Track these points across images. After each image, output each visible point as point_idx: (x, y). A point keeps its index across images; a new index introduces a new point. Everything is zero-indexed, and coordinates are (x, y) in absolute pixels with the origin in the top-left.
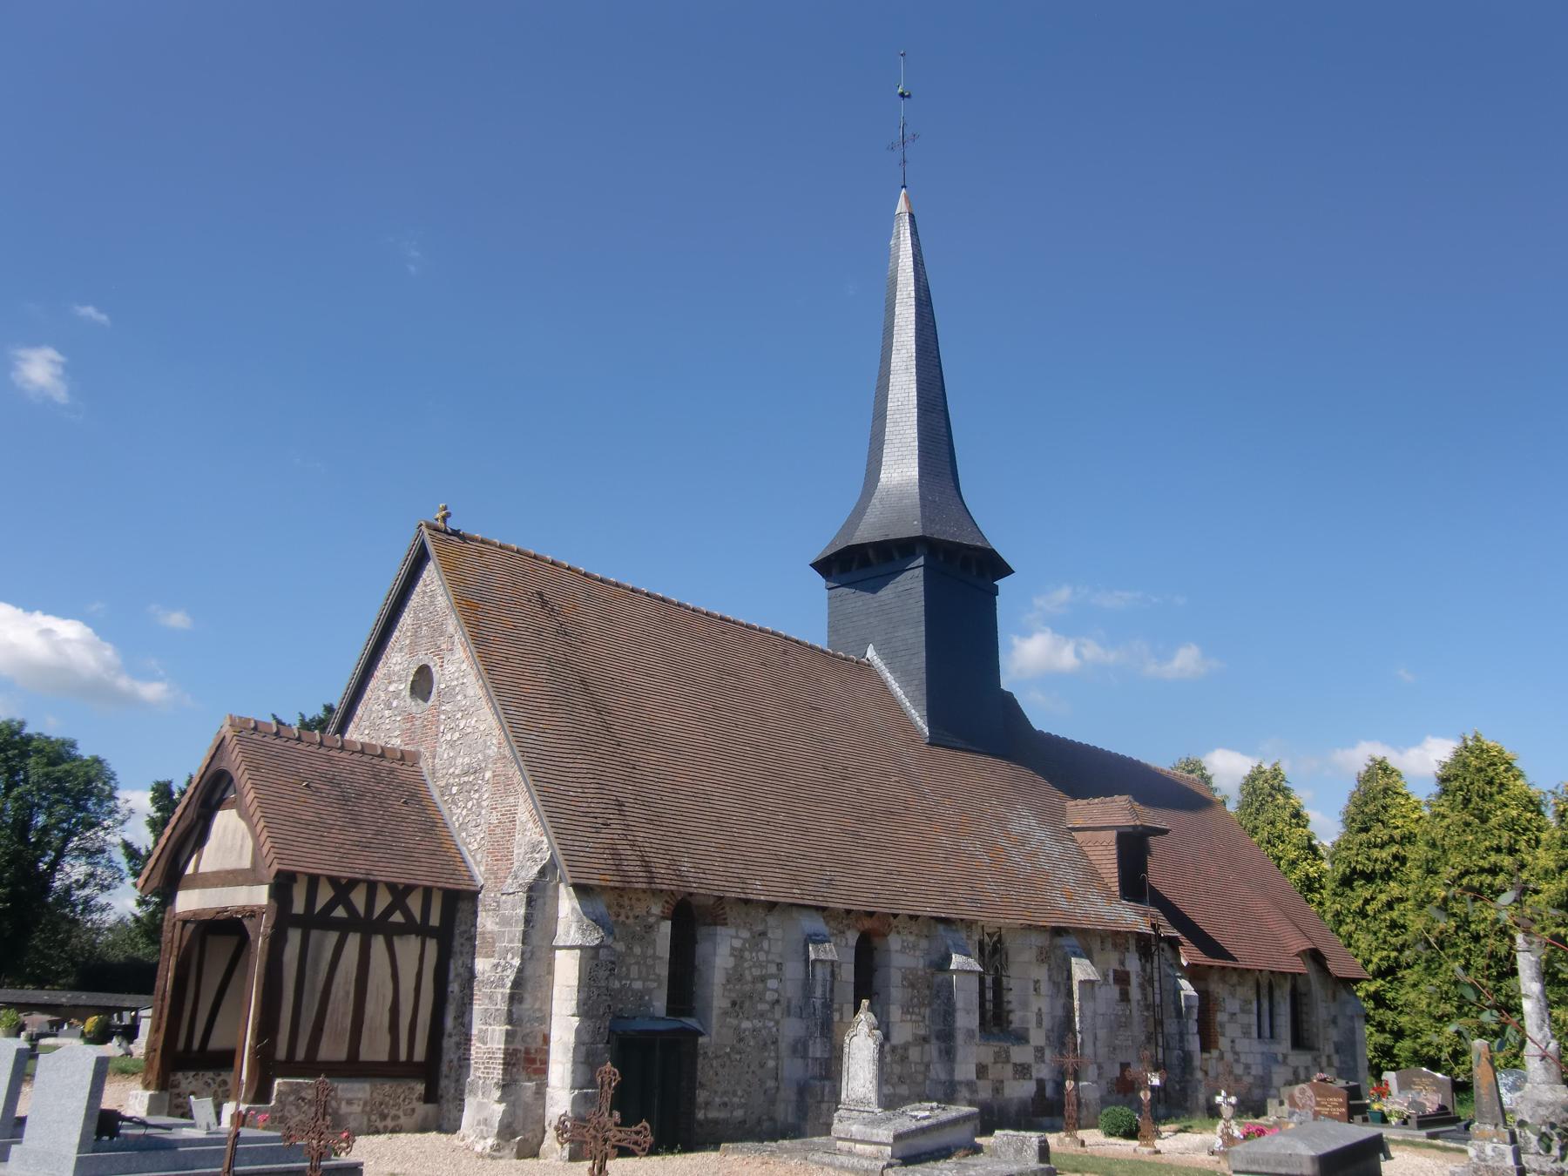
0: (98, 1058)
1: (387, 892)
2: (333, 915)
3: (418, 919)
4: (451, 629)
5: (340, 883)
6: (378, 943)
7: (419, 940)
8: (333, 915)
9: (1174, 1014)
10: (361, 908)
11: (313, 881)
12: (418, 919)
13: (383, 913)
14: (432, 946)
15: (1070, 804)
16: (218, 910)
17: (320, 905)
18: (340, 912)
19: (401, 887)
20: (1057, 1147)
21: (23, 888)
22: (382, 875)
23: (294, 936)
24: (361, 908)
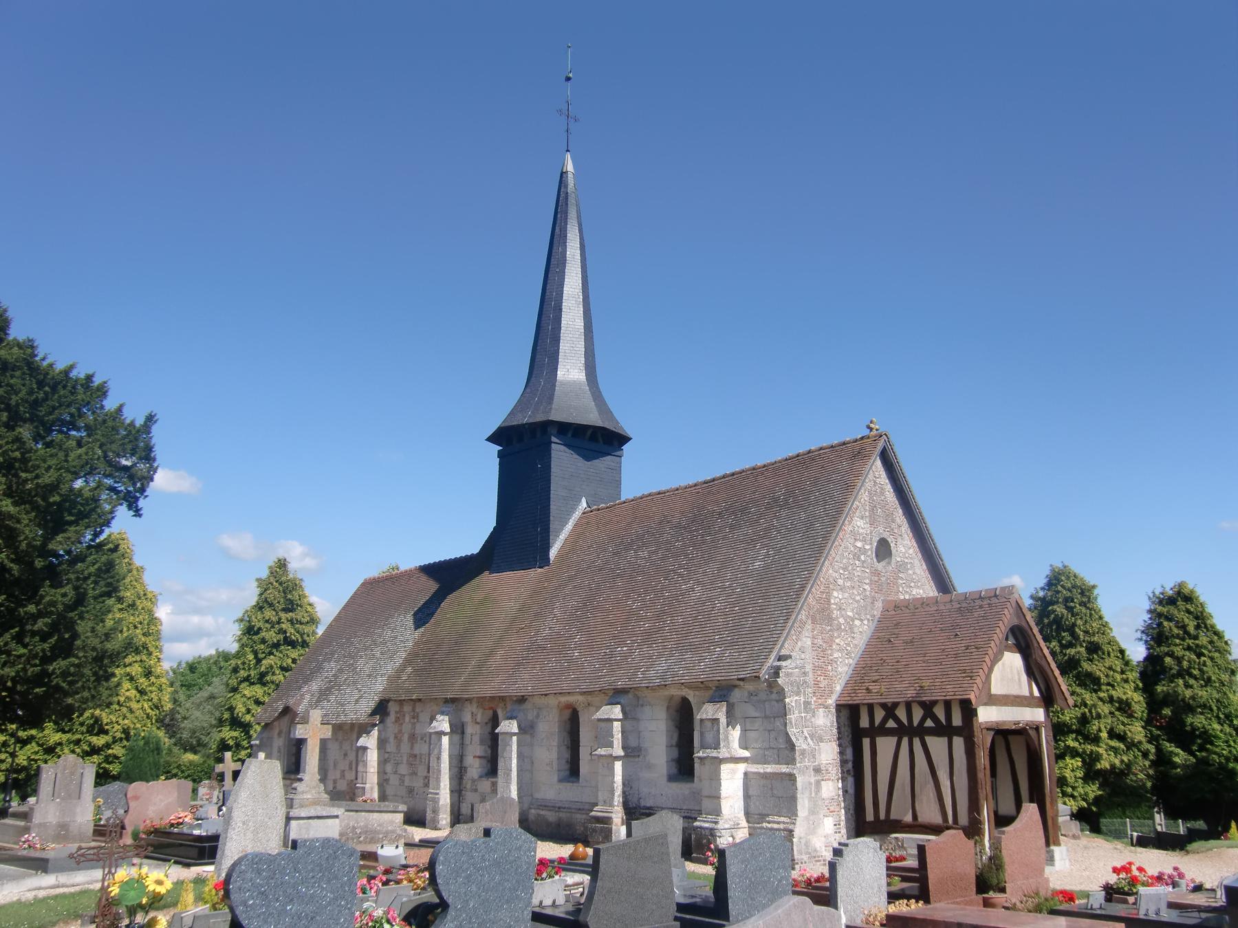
0: (984, 907)
1: (918, 706)
2: (896, 726)
3: (905, 722)
4: (898, 520)
5: (887, 706)
6: (917, 742)
7: (945, 739)
8: (896, 726)
9: (459, 732)
10: (904, 720)
11: (871, 707)
12: (905, 722)
13: (880, 723)
14: (958, 742)
15: (539, 842)
16: (465, 727)
17: (877, 721)
18: (891, 724)
19: (889, 705)
20: (698, 717)
21: (20, 713)
22: (875, 699)
23: (866, 742)
24: (904, 720)
